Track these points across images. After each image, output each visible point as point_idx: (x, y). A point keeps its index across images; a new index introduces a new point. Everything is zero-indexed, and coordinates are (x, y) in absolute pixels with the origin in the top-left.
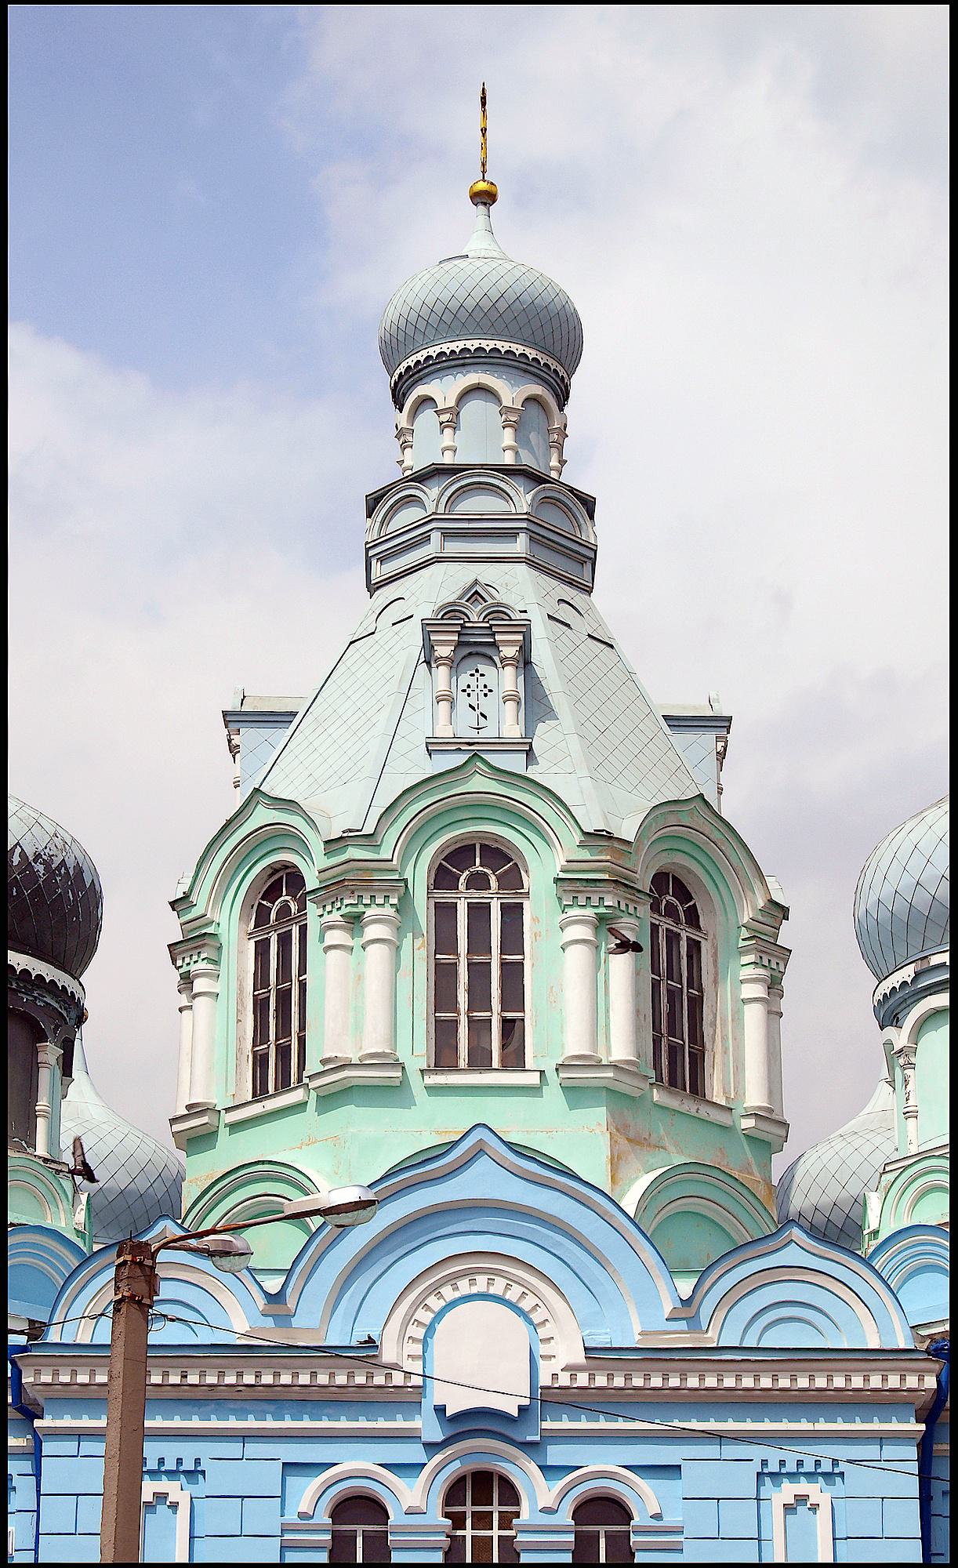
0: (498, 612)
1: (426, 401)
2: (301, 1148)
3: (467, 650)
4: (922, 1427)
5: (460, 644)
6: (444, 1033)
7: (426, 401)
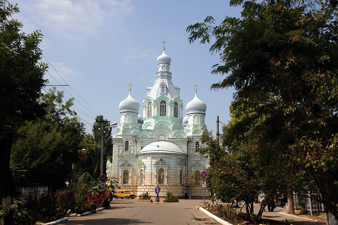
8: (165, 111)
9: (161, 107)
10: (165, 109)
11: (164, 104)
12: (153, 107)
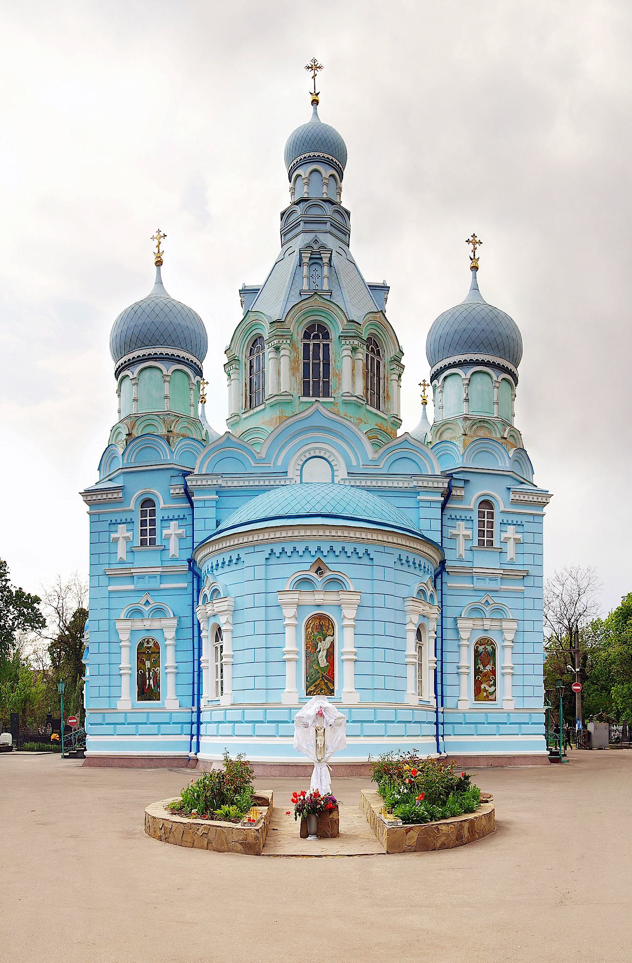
0: (323, 247)
1: (298, 176)
2: (473, 520)
3: (313, 261)
4: (443, 499)
5: (311, 258)
6: (306, 384)
7: (298, 176)
8: (327, 374)
9: (306, 356)
10: (327, 365)
11: (322, 342)
12: (271, 355)
